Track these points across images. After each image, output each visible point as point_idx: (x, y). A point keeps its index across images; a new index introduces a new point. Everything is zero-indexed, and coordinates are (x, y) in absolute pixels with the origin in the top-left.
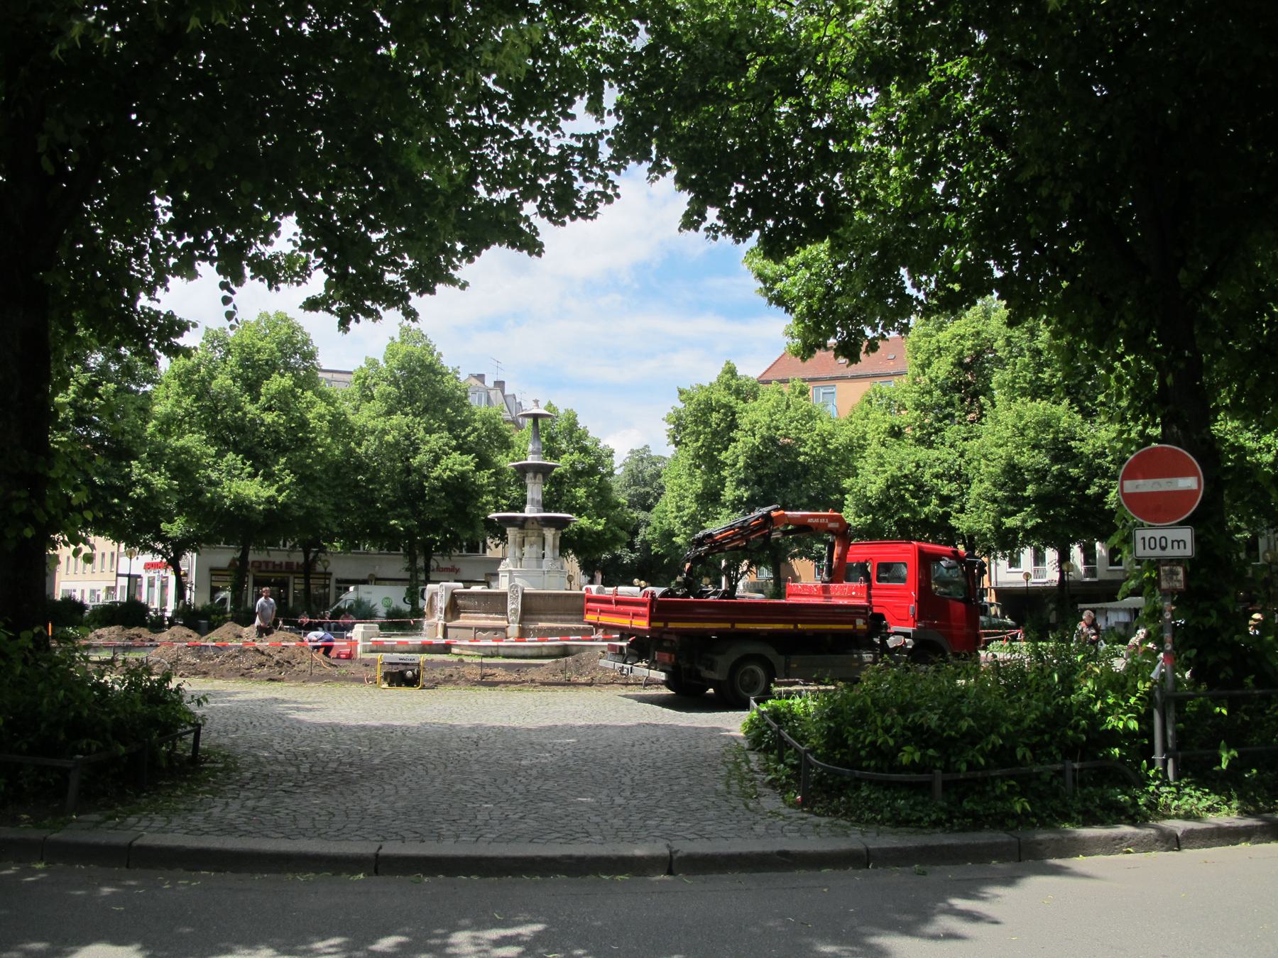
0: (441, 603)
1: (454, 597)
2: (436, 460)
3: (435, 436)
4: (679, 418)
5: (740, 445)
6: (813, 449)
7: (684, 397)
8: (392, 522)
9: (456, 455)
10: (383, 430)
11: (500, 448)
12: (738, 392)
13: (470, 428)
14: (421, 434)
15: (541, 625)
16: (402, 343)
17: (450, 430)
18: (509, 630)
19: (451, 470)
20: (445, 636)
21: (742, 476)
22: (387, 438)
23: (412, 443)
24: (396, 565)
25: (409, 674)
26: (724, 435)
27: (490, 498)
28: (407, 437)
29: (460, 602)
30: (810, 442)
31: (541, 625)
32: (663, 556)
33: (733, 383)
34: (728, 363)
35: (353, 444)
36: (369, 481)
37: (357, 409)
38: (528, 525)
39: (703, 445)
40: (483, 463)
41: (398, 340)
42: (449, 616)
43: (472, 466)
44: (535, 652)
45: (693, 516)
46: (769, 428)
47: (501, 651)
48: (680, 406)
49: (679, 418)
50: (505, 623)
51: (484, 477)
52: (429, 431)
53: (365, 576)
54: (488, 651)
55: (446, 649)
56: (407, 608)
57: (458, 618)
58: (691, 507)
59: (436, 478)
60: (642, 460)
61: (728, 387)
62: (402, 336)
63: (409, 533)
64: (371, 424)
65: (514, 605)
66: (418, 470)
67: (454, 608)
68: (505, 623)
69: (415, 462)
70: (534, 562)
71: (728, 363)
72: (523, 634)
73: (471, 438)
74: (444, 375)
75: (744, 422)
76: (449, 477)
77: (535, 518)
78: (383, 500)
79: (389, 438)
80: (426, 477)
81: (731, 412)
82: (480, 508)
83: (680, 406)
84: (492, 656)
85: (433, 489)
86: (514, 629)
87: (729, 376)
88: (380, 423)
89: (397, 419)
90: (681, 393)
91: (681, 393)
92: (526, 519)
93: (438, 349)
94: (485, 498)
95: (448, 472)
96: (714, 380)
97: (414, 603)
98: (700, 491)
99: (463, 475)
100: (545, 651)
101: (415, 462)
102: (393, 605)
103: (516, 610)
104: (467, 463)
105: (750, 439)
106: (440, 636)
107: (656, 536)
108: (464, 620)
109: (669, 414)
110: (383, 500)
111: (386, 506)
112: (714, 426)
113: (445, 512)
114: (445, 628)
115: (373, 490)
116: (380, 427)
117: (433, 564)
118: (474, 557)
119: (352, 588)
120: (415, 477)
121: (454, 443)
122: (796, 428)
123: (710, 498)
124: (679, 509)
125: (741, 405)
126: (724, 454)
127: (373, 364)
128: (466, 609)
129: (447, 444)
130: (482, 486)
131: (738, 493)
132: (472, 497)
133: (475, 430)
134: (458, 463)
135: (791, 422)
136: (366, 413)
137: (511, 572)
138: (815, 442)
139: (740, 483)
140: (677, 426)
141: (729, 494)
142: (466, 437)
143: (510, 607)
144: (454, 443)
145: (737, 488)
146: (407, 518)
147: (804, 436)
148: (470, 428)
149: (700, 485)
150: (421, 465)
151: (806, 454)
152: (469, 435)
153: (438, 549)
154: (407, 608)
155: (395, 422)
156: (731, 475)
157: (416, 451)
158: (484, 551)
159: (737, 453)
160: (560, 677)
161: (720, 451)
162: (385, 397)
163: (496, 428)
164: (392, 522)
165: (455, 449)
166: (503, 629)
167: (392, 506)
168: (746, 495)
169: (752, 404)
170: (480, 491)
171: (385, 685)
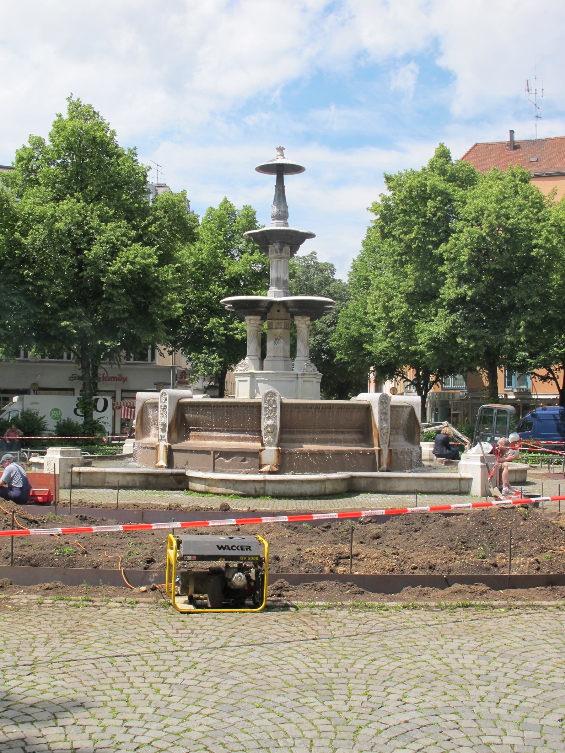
0: (164, 417)
1: (181, 409)
2: (114, 252)
3: (111, 225)
4: (387, 207)
5: (463, 236)
6: (547, 240)
7: (392, 184)
8: (63, 324)
9: (137, 245)
10: (53, 216)
11: (183, 242)
12: (452, 179)
13: (150, 218)
14: (96, 222)
15: (307, 447)
16: (71, 119)
17: (129, 220)
18: (264, 455)
19: (132, 263)
20: (170, 464)
21: (465, 271)
22: (58, 225)
23: (85, 234)
24: (64, 371)
25: (239, 579)
26: (440, 229)
27: (175, 296)
28: (80, 225)
29: (189, 416)
30: (544, 233)
31: (307, 447)
32: (347, 363)
33: (448, 167)
34: (442, 146)
35: (17, 235)
36: (37, 276)
37: (20, 196)
38: (273, 312)
39: (416, 238)
40: (166, 258)
41: (66, 116)
42: (174, 435)
43: (155, 260)
44: (316, 489)
45: (403, 318)
46: (498, 217)
47: (270, 488)
48: (389, 194)
49: (387, 207)
50: (258, 445)
51: (167, 273)
52: (104, 219)
53: (26, 386)
54: (250, 489)
55: (180, 482)
56: (80, 420)
57: (187, 438)
58: (400, 308)
59: (114, 273)
60: (308, 266)
61: (443, 172)
62: (71, 111)
63: (83, 338)
64: (38, 210)
65: (270, 421)
66: (94, 263)
67: (183, 422)
68: (258, 445)
69: (90, 255)
70: (281, 364)
71: (442, 146)
72: (284, 463)
73: (152, 229)
74: (119, 156)
75: (468, 211)
76: (130, 271)
77: (284, 303)
78: (53, 298)
79: (60, 225)
80: (104, 272)
81: (448, 199)
82: (163, 307)
83: (389, 194)
84: (256, 496)
85: (113, 285)
86: (270, 455)
87: (442, 160)
88: (49, 209)
89: (65, 205)
90: (388, 179)
91: (388, 179)
92: (272, 303)
93: (111, 128)
94: (170, 296)
95: (129, 266)
96: (426, 164)
97: (87, 415)
98: (411, 290)
99: (145, 269)
100: (329, 488)
101: (90, 255)
102: (64, 417)
103: (273, 426)
104: (150, 256)
105: (475, 229)
106: (162, 462)
107: (342, 342)
108: (194, 442)
109: (375, 204)
110: (53, 298)
111: (56, 306)
112: (429, 215)
113: (124, 311)
114: (170, 452)
115: (41, 287)
116: (49, 213)
117: (100, 372)
118: (143, 365)
119: (15, 399)
120: (88, 272)
121: (133, 233)
122: (527, 217)
123: (424, 297)
124: (387, 310)
125: (459, 193)
126: (443, 247)
127: (38, 143)
128: (198, 425)
129: (125, 235)
130: (166, 282)
131: (461, 291)
132: (154, 295)
133: (156, 219)
134: (139, 255)
135: (521, 210)
136: (31, 200)
137: (252, 375)
138: (550, 232)
139: (462, 279)
140: (384, 217)
141: (449, 291)
142: (146, 227)
143: (266, 422)
144: (133, 233)
145: (458, 285)
146: (80, 319)
147: (537, 226)
148: (150, 218)
149: (411, 283)
150: (97, 258)
151: (541, 247)
152: (150, 224)
153: (107, 355)
154: (80, 420)
155: (65, 207)
156: (451, 270)
157: (90, 241)
158: (153, 358)
159: (460, 243)
160: (469, 560)
161: (437, 245)
162: (52, 182)
163: (180, 218)
164: (63, 324)
165: (136, 240)
166: (256, 454)
167: (64, 305)
168: (470, 293)
169: (469, 193)
170: (165, 287)
171: (181, 602)
